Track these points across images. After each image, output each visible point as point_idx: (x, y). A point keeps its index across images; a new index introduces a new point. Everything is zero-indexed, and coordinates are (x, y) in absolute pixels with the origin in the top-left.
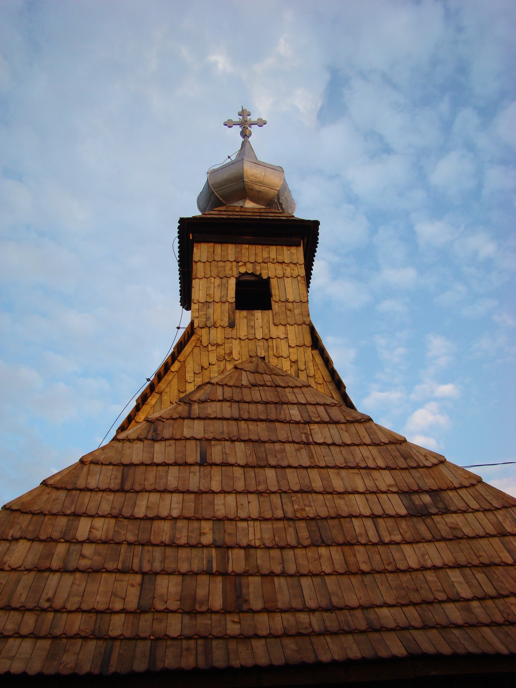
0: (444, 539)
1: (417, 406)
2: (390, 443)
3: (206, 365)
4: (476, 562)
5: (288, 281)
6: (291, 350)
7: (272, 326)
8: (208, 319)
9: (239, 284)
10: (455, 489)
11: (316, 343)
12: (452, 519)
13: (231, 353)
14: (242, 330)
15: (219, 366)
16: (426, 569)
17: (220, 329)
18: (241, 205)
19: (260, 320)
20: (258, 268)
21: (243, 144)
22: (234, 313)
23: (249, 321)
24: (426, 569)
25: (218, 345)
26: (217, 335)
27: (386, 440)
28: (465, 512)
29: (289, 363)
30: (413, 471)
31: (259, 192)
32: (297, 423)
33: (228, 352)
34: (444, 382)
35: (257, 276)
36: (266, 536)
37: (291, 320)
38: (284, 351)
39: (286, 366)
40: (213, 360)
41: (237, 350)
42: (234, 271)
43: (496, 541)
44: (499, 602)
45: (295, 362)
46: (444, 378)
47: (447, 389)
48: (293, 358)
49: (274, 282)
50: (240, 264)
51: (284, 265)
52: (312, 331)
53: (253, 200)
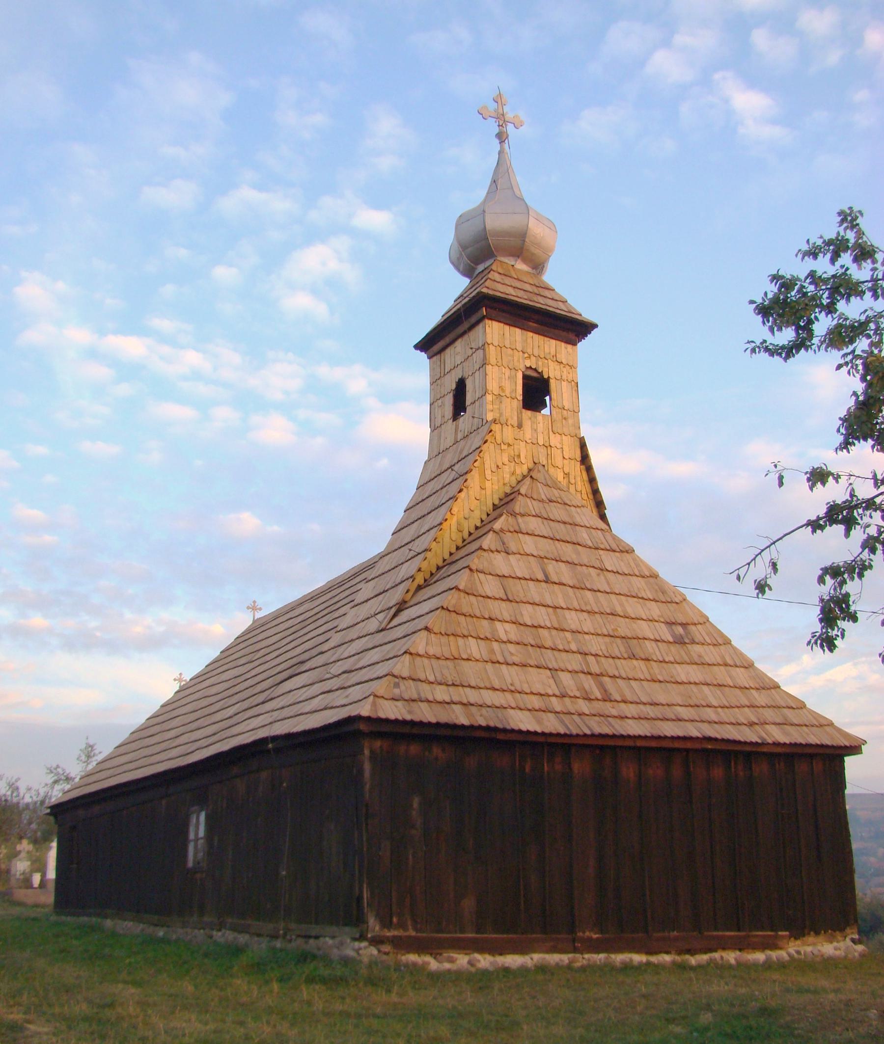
0: (696, 664)
1: (314, 235)
2: (651, 576)
3: (500, 464)
4: (715, 683)
5: (564, 384)
6: (565, 461)
7: (551, 433)
8: (501, 414)
9: (525, 377)
10: (695, 624)
11: (585, 458)
12: (697, 648)
13: (519, 456)
14: (528, 433)
15: (510, 467)
16: (690, 683)
17: (510, 427)
18: (513, 263)
19: (541, 424)
20: (540, 363)
21: (501, 153)
22: (521, 413)
23: (533, 423)
24: (690, 683)
25: (509, 445)
26: (509, 434)
27: (647, 574)
28: (703, 644)
29: (562, 474)
30: (669, 605)
31: (533, 254)
32: (590, 548)
33: (517, 453)
34: (377, 204)
35: (539, 373)
36: (603, 648)
37: (566, 431)
38: (559, 461)
39: (560, 476)
40: (506, 460)
41: (523, 450)
42: (523, 363)
43: (722, 668)
44: (731, 710)
45: (567, 475)
46: (377, 199)
47: (376, 220)
48: (566, 470)
49: (552, 383)
50: (526, 355)
51: (562, 366)
52: (583, 446)
53: (525, 261)
